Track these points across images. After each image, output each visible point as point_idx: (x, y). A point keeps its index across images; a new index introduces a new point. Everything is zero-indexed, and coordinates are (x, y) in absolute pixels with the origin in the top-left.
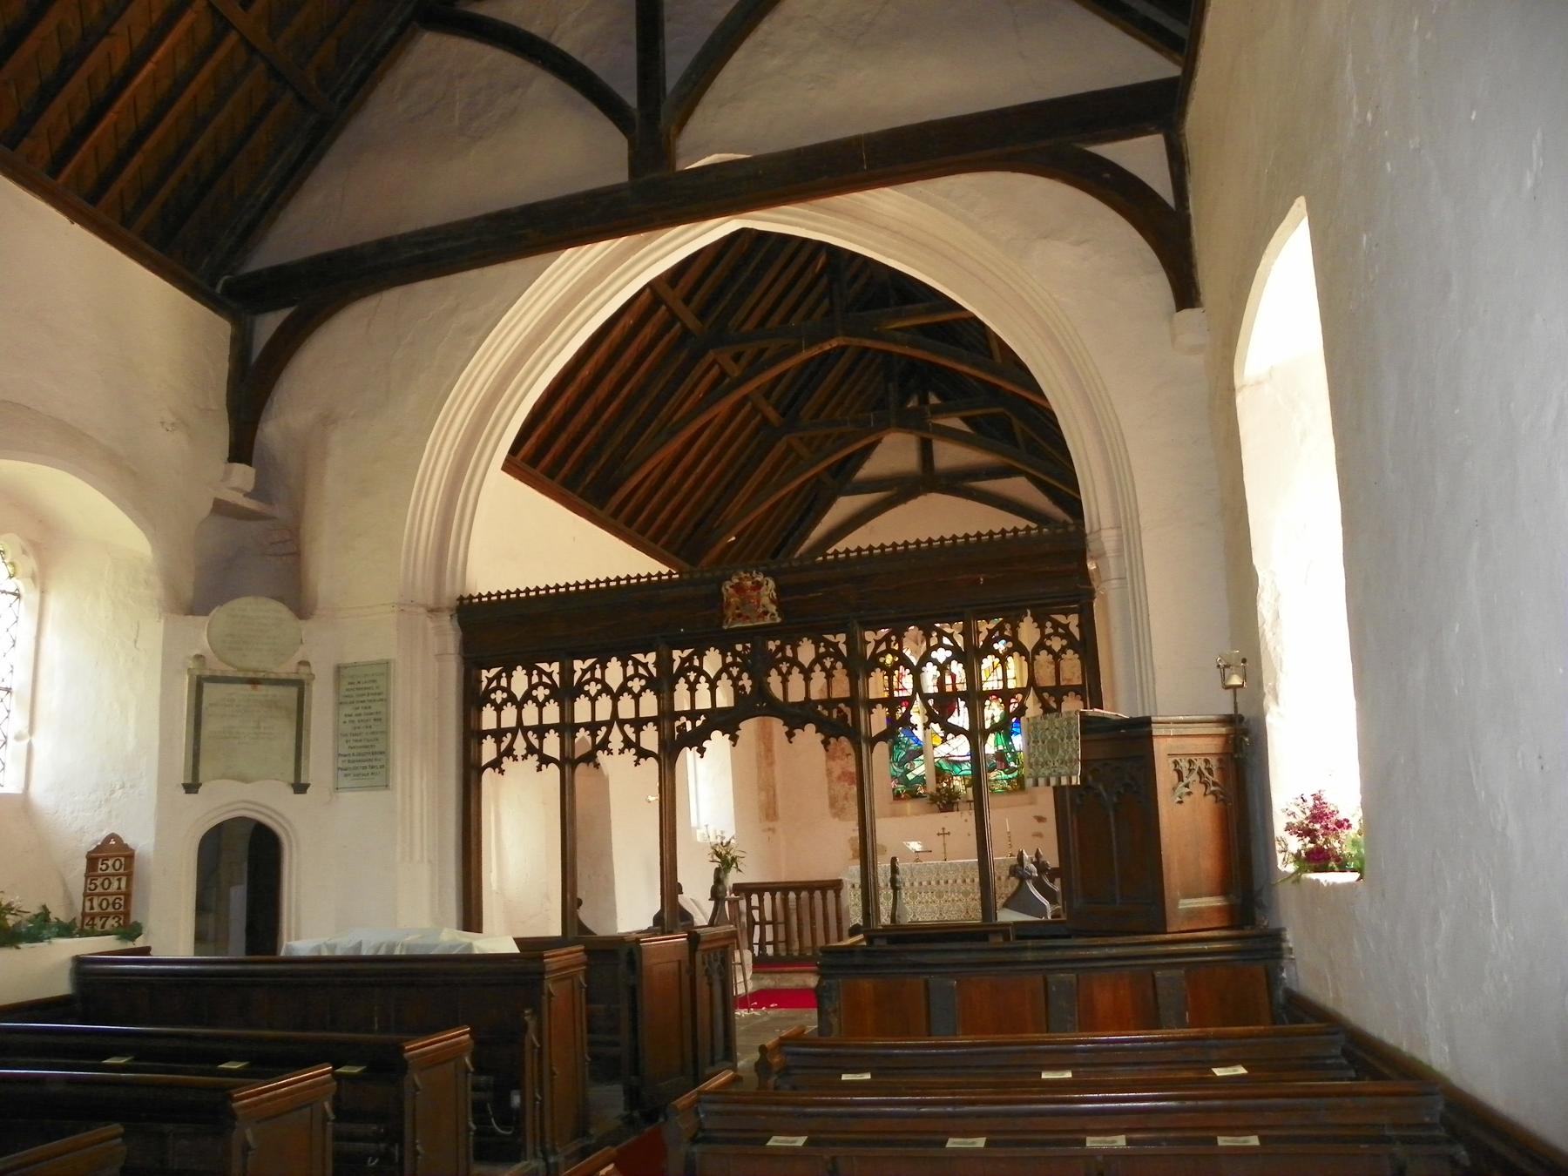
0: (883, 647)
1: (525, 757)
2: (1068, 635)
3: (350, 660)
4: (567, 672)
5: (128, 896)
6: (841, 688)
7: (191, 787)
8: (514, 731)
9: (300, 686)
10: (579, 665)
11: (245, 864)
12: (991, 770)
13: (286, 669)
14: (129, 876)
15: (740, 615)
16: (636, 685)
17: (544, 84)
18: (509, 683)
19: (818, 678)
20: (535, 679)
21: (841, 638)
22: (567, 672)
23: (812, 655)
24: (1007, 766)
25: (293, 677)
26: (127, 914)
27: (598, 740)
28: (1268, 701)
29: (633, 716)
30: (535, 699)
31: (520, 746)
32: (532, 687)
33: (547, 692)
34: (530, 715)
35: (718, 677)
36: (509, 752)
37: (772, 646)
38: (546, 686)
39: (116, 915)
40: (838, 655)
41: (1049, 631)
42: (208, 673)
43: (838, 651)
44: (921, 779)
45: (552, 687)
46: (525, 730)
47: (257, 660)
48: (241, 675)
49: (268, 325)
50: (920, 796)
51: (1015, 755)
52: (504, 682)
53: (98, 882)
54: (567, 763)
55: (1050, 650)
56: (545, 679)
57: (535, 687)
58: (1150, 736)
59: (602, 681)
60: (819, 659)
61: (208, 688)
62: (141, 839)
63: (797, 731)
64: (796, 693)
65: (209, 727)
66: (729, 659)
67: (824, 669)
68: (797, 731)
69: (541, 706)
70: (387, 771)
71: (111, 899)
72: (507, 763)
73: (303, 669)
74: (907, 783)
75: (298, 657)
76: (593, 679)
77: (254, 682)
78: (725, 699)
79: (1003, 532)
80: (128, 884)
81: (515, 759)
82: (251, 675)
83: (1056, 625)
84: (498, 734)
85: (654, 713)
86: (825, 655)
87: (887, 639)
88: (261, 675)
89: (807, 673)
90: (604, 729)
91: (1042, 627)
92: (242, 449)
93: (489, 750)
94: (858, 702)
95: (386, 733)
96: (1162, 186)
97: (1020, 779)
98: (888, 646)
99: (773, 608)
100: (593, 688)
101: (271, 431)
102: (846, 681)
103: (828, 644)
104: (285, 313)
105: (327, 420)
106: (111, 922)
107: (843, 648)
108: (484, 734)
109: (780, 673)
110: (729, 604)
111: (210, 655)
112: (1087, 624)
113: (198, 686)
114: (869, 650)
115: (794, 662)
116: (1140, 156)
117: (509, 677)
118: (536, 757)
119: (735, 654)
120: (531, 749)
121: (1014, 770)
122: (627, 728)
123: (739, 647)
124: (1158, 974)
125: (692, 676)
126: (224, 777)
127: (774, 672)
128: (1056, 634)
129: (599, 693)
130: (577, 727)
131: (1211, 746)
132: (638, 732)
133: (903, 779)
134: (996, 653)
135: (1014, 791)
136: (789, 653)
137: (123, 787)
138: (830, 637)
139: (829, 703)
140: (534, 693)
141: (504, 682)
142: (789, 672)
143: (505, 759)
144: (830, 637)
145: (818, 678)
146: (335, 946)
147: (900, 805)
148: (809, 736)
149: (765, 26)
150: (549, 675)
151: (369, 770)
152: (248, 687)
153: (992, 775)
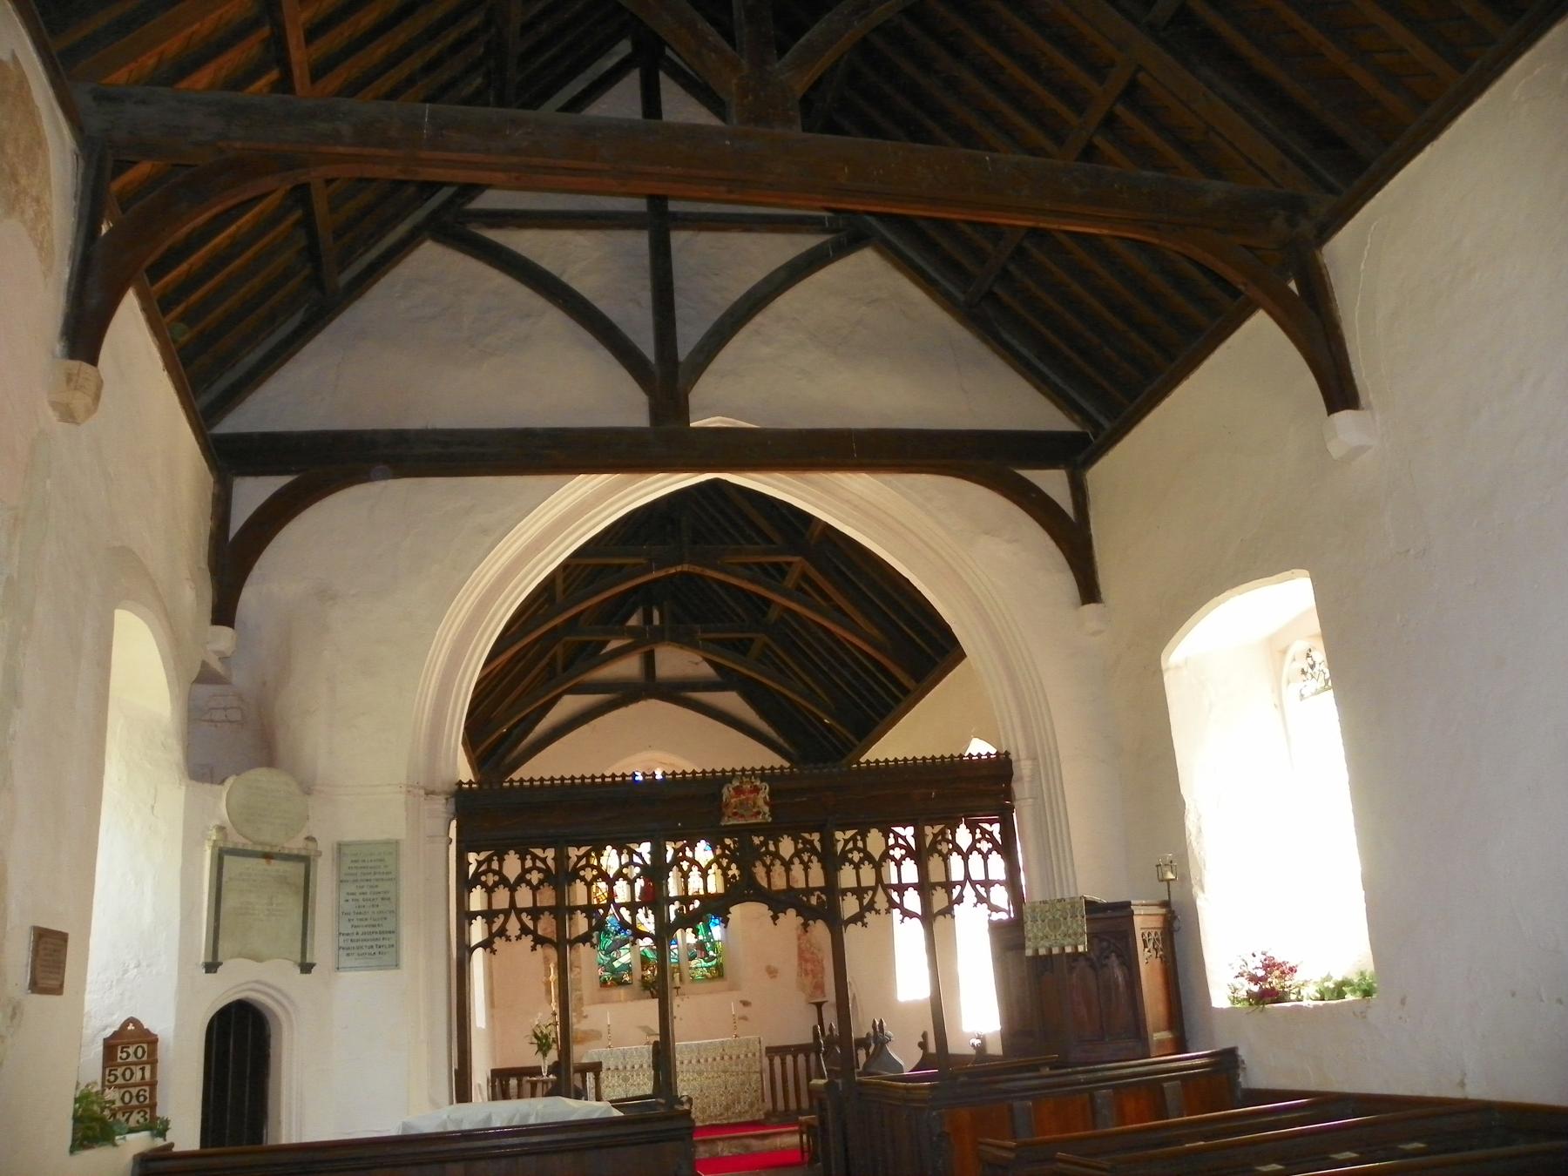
0: (850, 845)
1: (518, 938)
2: (992, 840)
3: (348, 838)
4: (561, 858)
5: (153, 1085)
6: (817, 877)
7: (211, 967)
8: (506, 913)
9: (305, 860)
10: (574, 853)
11: (240, 1045)
12: (692, 959)
13: (296, 845)
14: (153, 1063)
15: (735, 814)
16: (897, 853)
17: (554, 318)
18: (501, 866)
19: (797, 869)
20: (529, 863)
21: (816, 837)
22: (561, 858)
23: (792, 851)
24: (707, 954)
25: (303, 853)
26: (153, 1106)
27: (865, 902)
28: (1196, 890)
29: (855, 885)
30: (529, 883)
31: (513, 927)
32: (525, 871)
33: (541, 876)
34: (524, 897)
35: (709, 866)
36: (502, 932)
37: (757, 840)
38: (540, 870)
39: (140, 1108)
40: (813, 851)
41: (978, 836)
42: (230, 845)
43: (814, 848)
44: (627, 967)
45: (547, 871)
46: (519, 912)
47: (270, 836)
48: (259, 848)
49: (252, 493)
50: (626, 983)
51: (713, 944)
52: (495, 866)
53: (119, 1072)
54: (927, 918)
55: (980, 852)
56: (539, 864)
57: (529, 871)
58: (1132, 913)
59: (499, 873)
60: (798, 853)
61: (227, 859)
62: (160, 1023)
63: (781, 915)
64: (779, 882)
65: (229, 902)
66: (718, 852)
67: (802, 862)
68: (781, 915)
69: (535, 889)
70: (397, 952)
71: (134, 1091)
72: (499, 943)
73: (311, 845)
74: (613, 971)
75: (304, 834)
76: (855, 848)
77: (268, 856)
78: (715, 885)
79: (684, 773)
80: (153, 1072)
81: (508, 939)
82: (267, 849)
83: (984, 832)
84: (859, 891)
85: (916, 880)
86: (803, 851)
87: (853, 838)
88: (276, 850)
89: (787, 865)
90: (502, 917)
91: (973, 833)
92: (224, 613)
93: (477, 932)
94: (832, 890)
95: (395, 913)
96: (1066, 504)
97: (719, 967)
98: (489, 866)
99: (766, 809)
100: (491, 879)
101: (250, 597)
102: (821, 873)
103: (806, 842)
104: (285, 480)
105: (325, 594)
106: (136, 1117)
107: (818, 845)
108: (844, 892)
109: (764, 864)
110: (727, 805)
111: (228, 824)
112: (1008, 832)
113: (220, 856)
114: (840, 847)
115: (776, 855)
116: (1052, 482)
117: (501, 861)
118: (530, 937)
119: (725, 847)
120: (525, 930)
121: (713, 958)
122: (524, 916)
123: (728, 841)
124: (1017, 1104)
125: (685, 865)
126: (240, 955)
127: (758, 864)
128: (984, 837)
129: (862, 861)
130: (573, 910)
131: (1159, 924)
132: (535, 919)
133: (609, 967)
134: (851, 862)
135: (713, 978)
136: (772, 848)
137: (138, 966)
138: (807, 835)
139: (809, 891)
140: (528, 876)
141: (495, 866)
142: (772, 864)
143: (497, 940)
144: (807, 835)
145: (797, 869)
146: (528, 1115)
147: (605, 993)
148: (790, 918)
149: (758, 319)
150: (544, 860)
151: (376, 950)
152: (263, 861)
153: (693, 963)
